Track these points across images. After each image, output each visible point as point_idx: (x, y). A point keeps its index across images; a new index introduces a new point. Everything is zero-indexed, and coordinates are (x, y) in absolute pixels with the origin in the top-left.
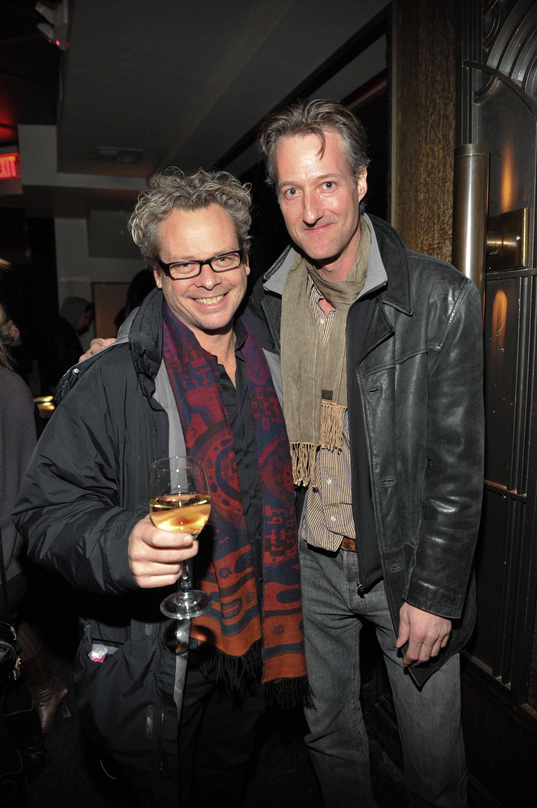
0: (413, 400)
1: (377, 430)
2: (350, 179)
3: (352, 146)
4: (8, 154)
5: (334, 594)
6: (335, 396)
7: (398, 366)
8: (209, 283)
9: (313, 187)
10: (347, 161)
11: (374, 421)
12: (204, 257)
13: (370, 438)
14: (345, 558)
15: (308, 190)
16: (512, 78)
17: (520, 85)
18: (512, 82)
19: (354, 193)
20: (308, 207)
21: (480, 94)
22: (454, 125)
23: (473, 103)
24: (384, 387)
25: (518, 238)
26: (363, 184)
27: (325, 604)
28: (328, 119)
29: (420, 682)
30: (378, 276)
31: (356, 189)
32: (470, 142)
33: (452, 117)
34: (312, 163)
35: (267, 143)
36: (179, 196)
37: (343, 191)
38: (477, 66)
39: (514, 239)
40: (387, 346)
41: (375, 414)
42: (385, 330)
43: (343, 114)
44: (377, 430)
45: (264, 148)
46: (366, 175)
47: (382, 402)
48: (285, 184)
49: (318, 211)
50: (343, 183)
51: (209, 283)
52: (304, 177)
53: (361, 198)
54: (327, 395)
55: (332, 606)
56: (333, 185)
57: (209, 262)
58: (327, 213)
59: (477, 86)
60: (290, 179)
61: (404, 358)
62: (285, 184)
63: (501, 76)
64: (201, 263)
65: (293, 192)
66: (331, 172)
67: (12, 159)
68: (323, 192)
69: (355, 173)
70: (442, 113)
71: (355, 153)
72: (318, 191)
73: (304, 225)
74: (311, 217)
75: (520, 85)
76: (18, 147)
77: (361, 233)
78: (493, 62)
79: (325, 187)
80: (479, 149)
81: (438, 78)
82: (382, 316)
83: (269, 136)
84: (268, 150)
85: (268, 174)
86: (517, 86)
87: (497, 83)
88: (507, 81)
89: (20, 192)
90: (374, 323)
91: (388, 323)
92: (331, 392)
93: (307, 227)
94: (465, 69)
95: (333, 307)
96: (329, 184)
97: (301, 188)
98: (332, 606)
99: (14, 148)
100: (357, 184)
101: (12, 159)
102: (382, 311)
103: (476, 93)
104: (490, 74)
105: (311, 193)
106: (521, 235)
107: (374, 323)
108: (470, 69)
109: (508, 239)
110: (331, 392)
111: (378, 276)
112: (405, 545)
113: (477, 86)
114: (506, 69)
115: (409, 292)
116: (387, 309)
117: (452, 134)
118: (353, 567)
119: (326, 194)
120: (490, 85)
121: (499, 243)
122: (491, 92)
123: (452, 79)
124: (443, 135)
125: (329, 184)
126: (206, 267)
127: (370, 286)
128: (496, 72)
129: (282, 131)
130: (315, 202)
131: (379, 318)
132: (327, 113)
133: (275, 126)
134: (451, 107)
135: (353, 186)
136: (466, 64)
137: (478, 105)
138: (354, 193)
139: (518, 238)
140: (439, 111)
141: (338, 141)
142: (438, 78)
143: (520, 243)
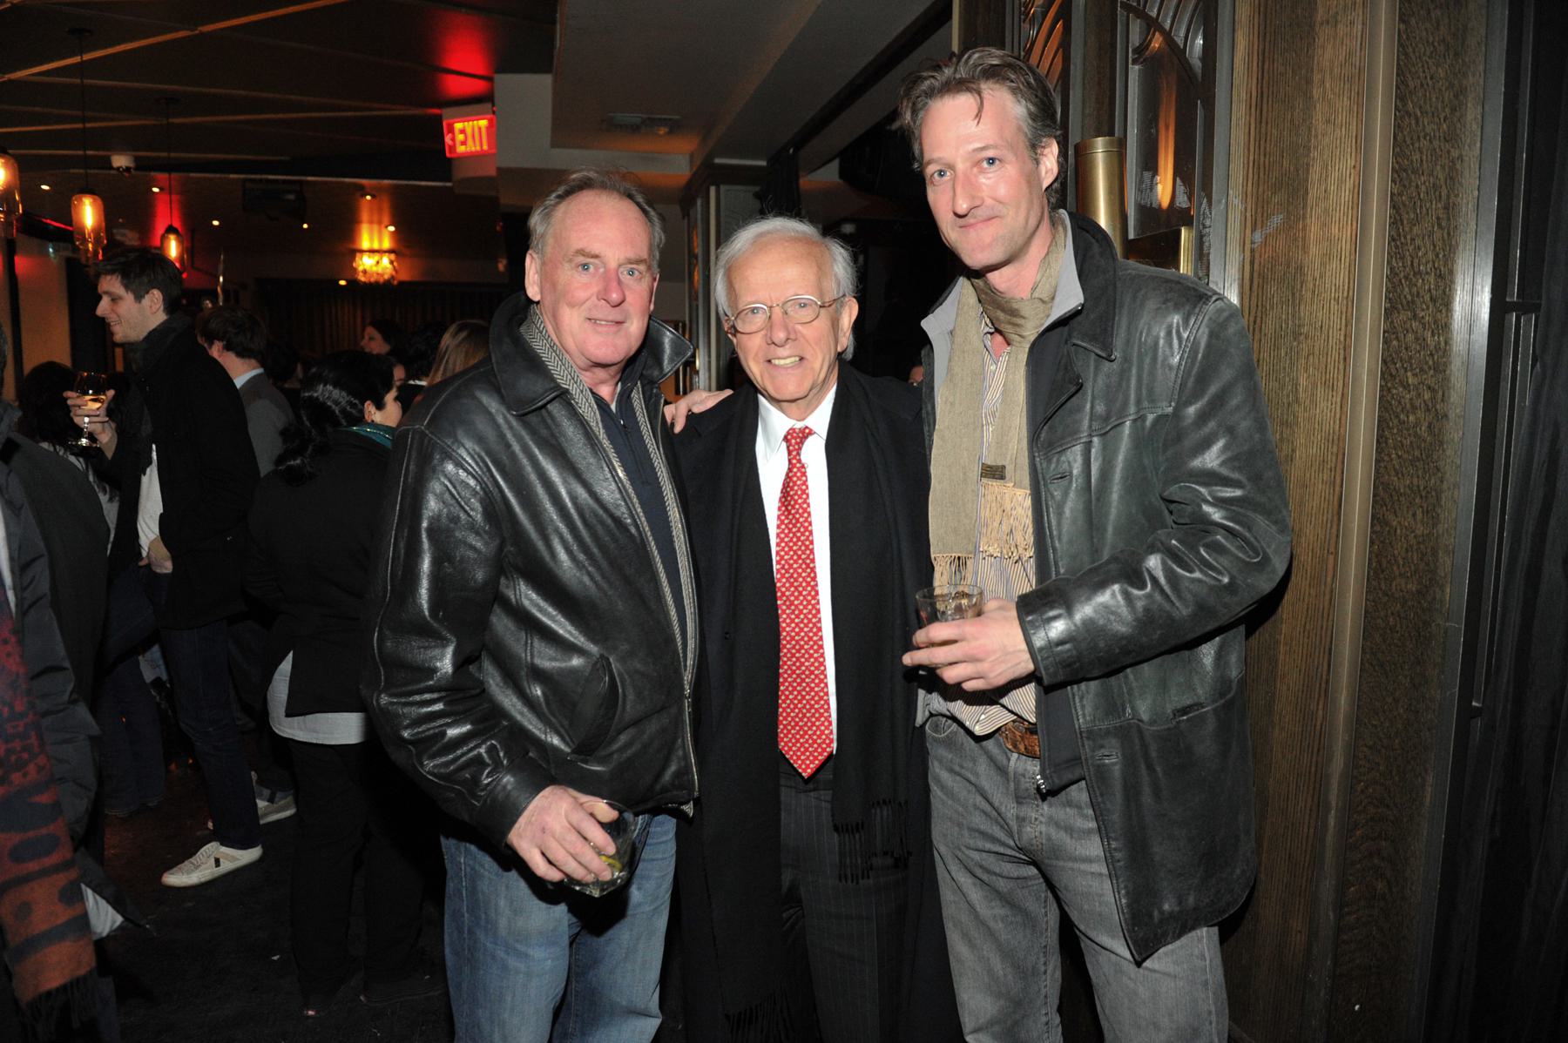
0: (1121, 497)
1: (1065, 539)
2: (1027, 153)
5: (997, 822)
6: (1009, 472)
7: (1095, 439)
10: (1019, 129)
11: (1059, 524)
13: (1054, 550)
14: (1012, 763)
19: (1032, 178)
20: (959, 190)
24: (1075, 472)
27: (984, 835)
29: (1140, 954)
30: (1071, 296)
35: (915, 112)
37: (1011, 170)
40: (1080, 409)
41: (1060, 514)
44: (1065, 539)
47: (1072, 495)
49: (973, 198)
50: (1010, 156)
54: (994, 472)
55: (994, 840)
58: (989, 201)
61: (1108, 429)
65: (941, 173)
67: (483, 123)
68: (982, 171)
74: (963, 207)
79: (985, 164)
89: (493, 173)
98: (994, 840)
100: (1037, 162)
101: (483, 123)
111: (1071, 296)
112: (1126, 257)
115: (1304, 238)
125: (991, 161)
127: (1058, 311)
129: (932, 93)
130: (971, 185)
135: (1030, 165)
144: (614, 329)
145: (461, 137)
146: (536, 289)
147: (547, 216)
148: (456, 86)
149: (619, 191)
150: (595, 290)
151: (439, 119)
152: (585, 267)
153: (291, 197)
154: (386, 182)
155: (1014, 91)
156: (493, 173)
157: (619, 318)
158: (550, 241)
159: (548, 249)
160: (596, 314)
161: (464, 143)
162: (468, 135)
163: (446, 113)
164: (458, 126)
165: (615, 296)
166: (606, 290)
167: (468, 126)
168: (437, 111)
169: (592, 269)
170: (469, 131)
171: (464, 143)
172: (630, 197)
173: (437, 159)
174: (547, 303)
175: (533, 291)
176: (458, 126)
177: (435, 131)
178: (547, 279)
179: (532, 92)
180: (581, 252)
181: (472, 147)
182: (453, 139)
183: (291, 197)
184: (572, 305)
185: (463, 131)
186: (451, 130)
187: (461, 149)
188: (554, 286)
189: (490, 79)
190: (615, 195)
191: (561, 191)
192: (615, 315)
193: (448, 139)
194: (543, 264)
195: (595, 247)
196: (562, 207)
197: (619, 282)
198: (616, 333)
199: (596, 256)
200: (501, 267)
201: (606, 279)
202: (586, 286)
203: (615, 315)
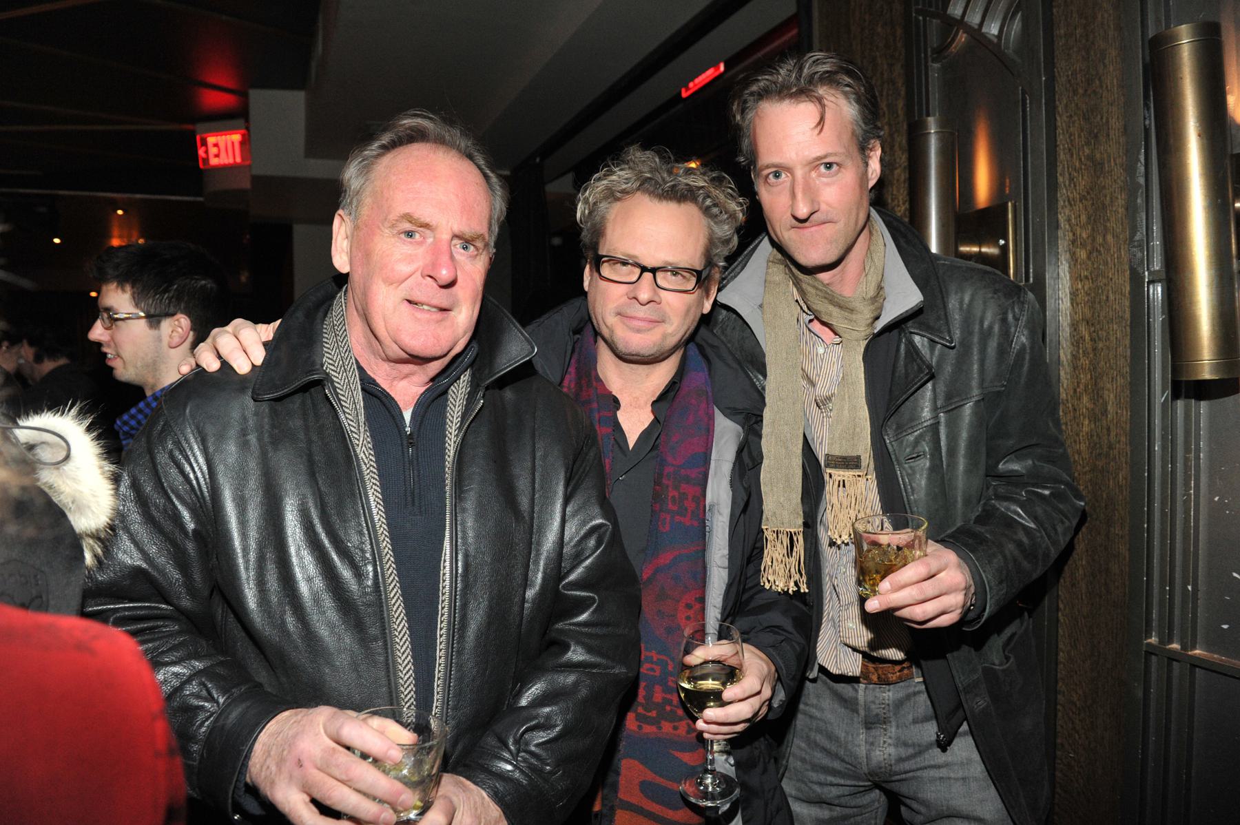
3: (862, 113)
4: (232, 130)
8: (644, 296)
9: (807, 169)
10: (853, 133)
12: (649, 262)
15: (799, 173)
16: (984, 30)
17: (995, 40)
18: (984, 36)
19: (864, 177)
20: (799, 196)
21: (940, 52)
22: (903, 93)
23: (930, 63)
25: (1002, 242)
26: (875, 167)
28: (829, 79)
30: (905, 295)
31: (866, 171)
32: (928, 115)
33: (900, 82)
34: (804, 137)
35: (743, 112)
36: (650, 178)
37: (848, 176)
38: (933, 16)
39: (996, 244)
42: (920, 370)
43: (849, 73)
45: (738, 117)
46: (879, 152)
48: (768, 167)
49: (813, 201)
50: (849, 163)
51: (644, 296)
52: (793, 156)
53: (872, 183)
56: (835, 167)
57: (654, 271)
59: (934, 41)
60: (776, 160)
62: (768, 167)
63: (968, 29)
64: (644, 269)
65: (777, 175)
66: (830, 151)
67: (236, 138)
68: (820, 175)
69: (863, 149)
70: (885, 76)
71: (865, 123)
72: (814, 174)
73: (794, 221)
74: (803, 211)
75: (995, 40)
76: (247, 121)
77: (871, 233)
78: (956, 10)
79: (822, 169)
80: (943, 124)
81: (879, 29)
82: (913, 350)
83: (745, 102)
84: (743, 118)
85: (741, 151)
86: (990, 41)
87: (962, 37)
88: (976, 34)
90: (901, 362)
91: (923, 362)
92: (859, 458)
93: (797, 224)
94: (917, 20)
95: (836, 334)
96: (829, 166)
97: (789, 170)
99: (241, 122)
100: (867, 164)
101: (236, 138)
102: (911, 343)
103: (933, 50)
104: (952, 25)
105: (804, 178)
106: (1006, 239)
107: (901, 362)
108: (924, 20)
109: (988, 245)
110: (859, 458)
111: (905, 295)
113: (934, 41)
114: (974, 19)
115: (946, 314)
116: (917, 339)
117: (901, 104)
118: (873, 706)
119: (824, 180)
120: (953, 40)
121: (975, 249)
122: (954, 48)
123: (899, 31)
124: (888, 106)
125: (829, 166)
126: (648, 275)
128: (961, 23)
129: (763, 94)
131: (908, 352)
132: (827, 72)
133: (754, 88)
134: (898, 69)
136: (918, 12)
137: (936, 65)
138: (864, 177)
139: (1002, 242)
140: (882, 74)
141: (843, 108)
142: (879, 29)
143: (1004, 249)
144: (439, 315)
145: (213, 150)
146: (345, 258)
147: (366, 169)
148: (213, 100)
149: (459, 150)
150: (420, 263)
151: (193, 135)
152: (410, 234)
153: (43, 210)
154: (138, 196)
155: (846, 94)
156: (247, 185)
157: (445, 305)
158: (367, 200)
159: (365, 211)
160: (417, 296)
161: (217, 156)
162: (222, 148)
163: (199, 127)
164: (211, 140)
165: (445, 274)
166: (435, 265)
167: (221, 140)
168: (190, 127)
169: (417, 236)
170: (222, 145)
171: (217, 156)
172: (470, 157)
173: (190, 170)
174: (356, 279)
175: (341, 262)
176: (211, 140)
177: (188, 146)
178: (360, 247)
179: (282, 109)
180: (408, 217)
181: (225, 160)
182: (206, 152)
183: (43, 210)
184: (389, 282)
185: (216, 145)
186: (204, 143)
187: (214, 161)
188: (368, 255)
189: (244, 95)
190: (454, 152)
191: (386, 139)
192: (441, 298)
193: (201, 152)
194: (356, 228)
195: (425, 213)
196: (387, 159)
197: (452, 257)
198: (438, 322)
199: (426, 226)
200: (243, 279)
201: (435, 250)
202: (410, 259)
203: (441, 298)
